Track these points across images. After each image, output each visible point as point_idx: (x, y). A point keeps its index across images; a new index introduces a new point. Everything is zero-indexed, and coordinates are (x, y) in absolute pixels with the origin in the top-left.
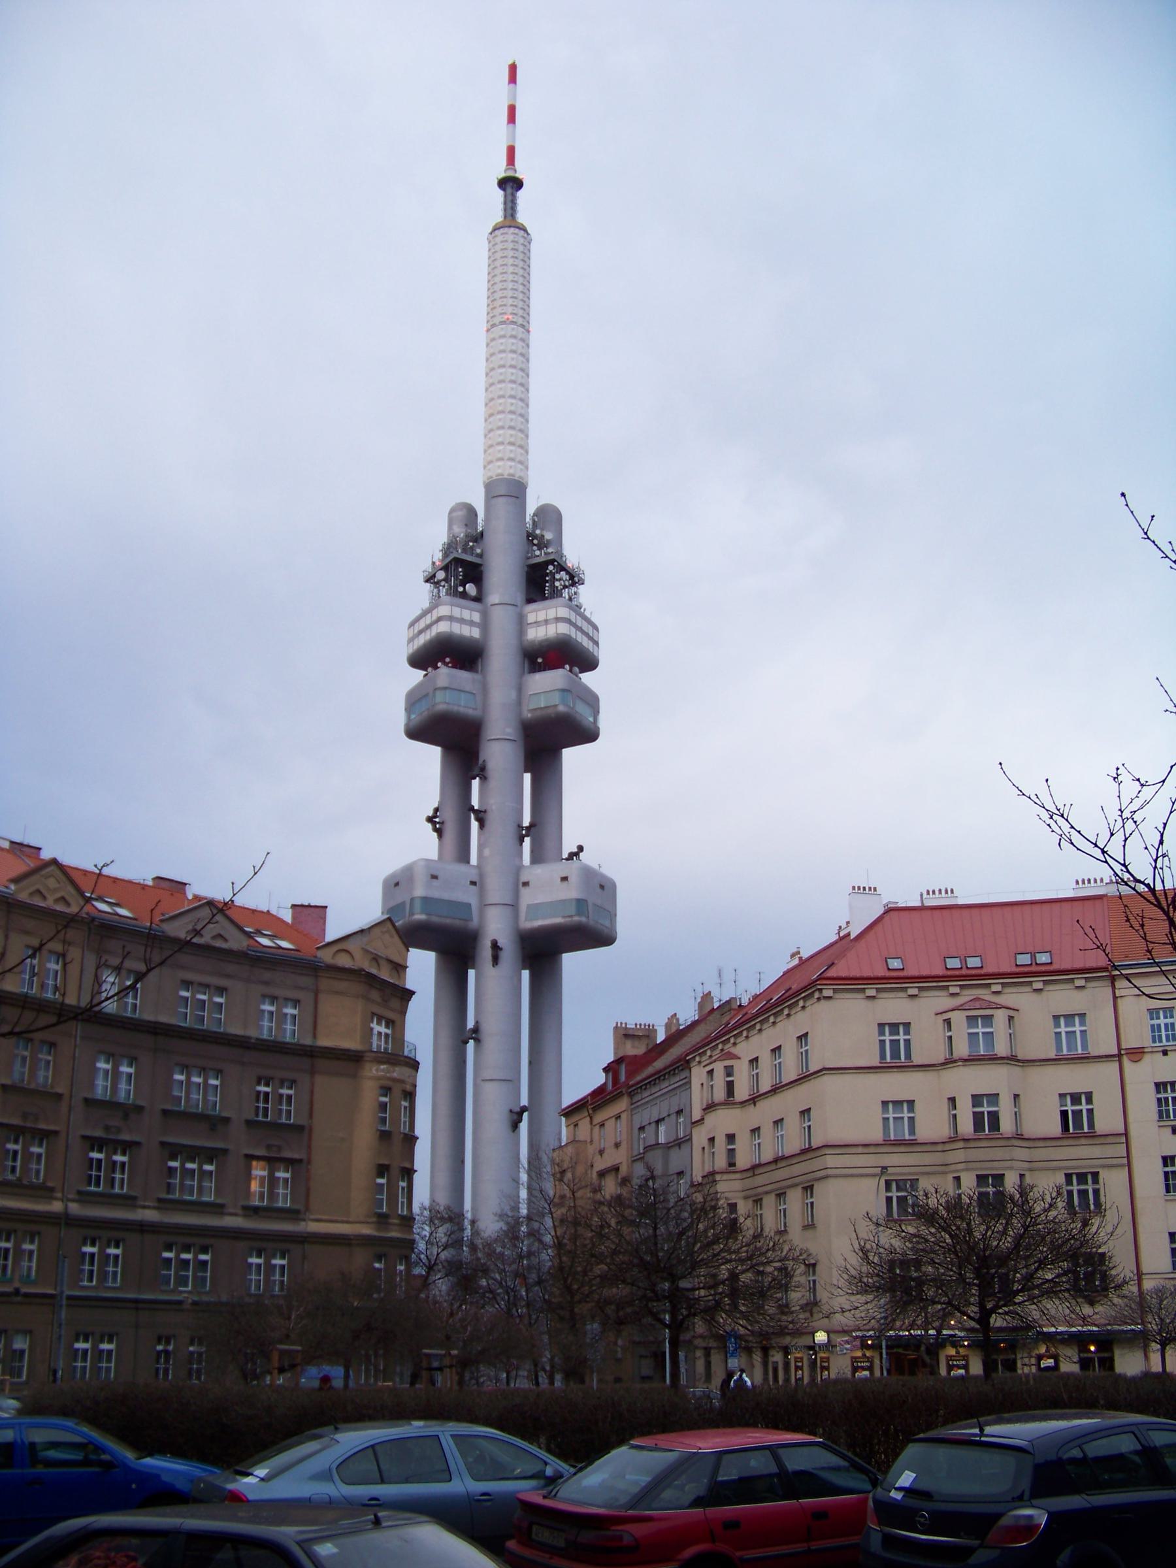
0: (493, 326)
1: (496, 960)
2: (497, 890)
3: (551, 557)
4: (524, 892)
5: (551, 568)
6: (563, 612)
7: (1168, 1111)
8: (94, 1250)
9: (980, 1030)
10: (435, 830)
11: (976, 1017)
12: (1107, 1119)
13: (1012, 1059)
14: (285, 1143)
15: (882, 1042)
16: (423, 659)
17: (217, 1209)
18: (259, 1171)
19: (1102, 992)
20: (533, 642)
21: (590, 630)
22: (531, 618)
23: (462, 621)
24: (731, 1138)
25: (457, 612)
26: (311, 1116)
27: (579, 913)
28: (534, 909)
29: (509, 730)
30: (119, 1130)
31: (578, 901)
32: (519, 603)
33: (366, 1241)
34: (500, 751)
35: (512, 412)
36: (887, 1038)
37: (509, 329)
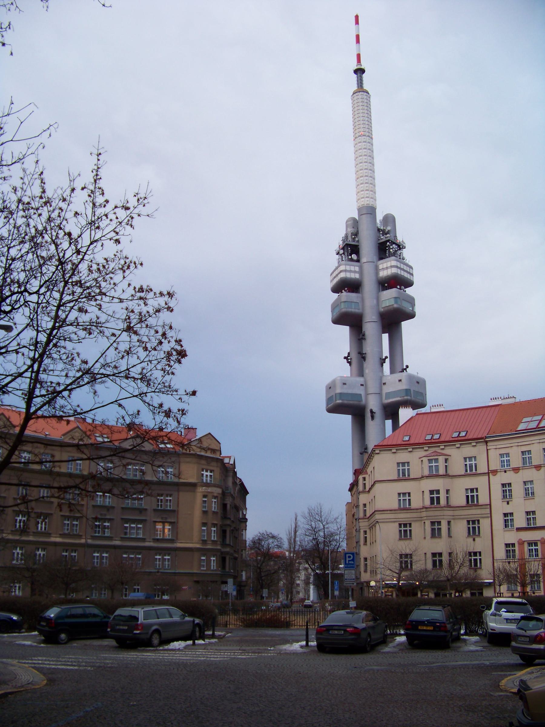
0: (356, 138)
1: (373, 418)
2: (372, 388)
3: (388, 239)
4: (384, 387)
5: (388, 243)
6: (394, 263)
7: (506, 495)
8: (98, 555)
9: (434, 464)
10: (348, 362)
11: (432, 459)
12: (483, 499)
13: (446, 475)
14: (168, 515)
15: (399, 470)
16: (336, 289)
17: (143, 540)
18: (159, 526)
19: (482, 447)
20: (382, 277)
21: (408, 269)
22: (381, 267)
23: (350, 271)
24: (365, 505)
25: (348, 268)
26: (178, 506)
27: (407, 395)
28: (388, 395)
29: (374, 317)
30: (105, 515)
31: (406, 390)
32: (375, 260)
33: (198, 550)
34: (371, 327)
35: (366, 176)
36: (401, 468)
37: (363, 139)
